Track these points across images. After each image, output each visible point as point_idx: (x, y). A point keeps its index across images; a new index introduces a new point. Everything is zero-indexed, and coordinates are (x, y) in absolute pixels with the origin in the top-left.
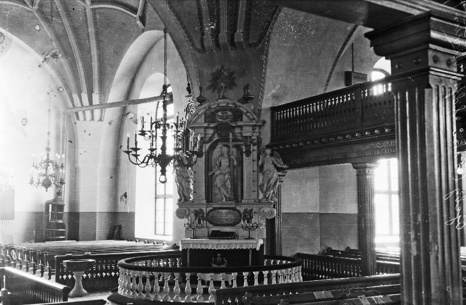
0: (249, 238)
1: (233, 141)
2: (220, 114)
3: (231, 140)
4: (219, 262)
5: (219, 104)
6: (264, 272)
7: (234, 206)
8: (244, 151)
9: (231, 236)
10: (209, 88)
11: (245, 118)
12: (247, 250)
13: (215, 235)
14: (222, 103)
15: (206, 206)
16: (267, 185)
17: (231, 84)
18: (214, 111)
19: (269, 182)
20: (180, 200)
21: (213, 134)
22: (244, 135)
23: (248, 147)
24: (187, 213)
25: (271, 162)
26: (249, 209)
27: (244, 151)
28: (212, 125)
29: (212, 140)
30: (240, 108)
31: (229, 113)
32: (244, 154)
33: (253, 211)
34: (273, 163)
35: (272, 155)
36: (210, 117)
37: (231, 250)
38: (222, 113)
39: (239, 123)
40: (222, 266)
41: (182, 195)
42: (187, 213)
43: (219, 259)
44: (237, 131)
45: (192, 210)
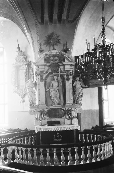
0: (71, 124)
1: (60, 73)
2: (52, 58)
3: (59, 73)
4: (58, 137)
5: (51, 53)
6: (34, 149)
7: (61, 107)
8: (66, 78)
9: (58, 123)
10: (44, 44)
11: (66, 60)
12: (73, 130)
13: (50, 123)
14: (54, 52)
16: (78, 96)
17: (58, 42)
18: (48, 56)
19: (79, 94)
20: (31, 105)
21: (49, 69)
22: (66, 69)
23: (68, 76)
25: (79, 84)
26: (70, 108)
27: (66, 78)
30: (64, 55)
31: (57, 58)
32: (66, 80)
33: (72, 110)
34: (80, 85)
35: (79, 80)
36: (47, 60)
37: (64, 131)
38: (53, 58)
40: (60, 140)
41: (31, 102)
44: (62, 67)
45: (38, 110)
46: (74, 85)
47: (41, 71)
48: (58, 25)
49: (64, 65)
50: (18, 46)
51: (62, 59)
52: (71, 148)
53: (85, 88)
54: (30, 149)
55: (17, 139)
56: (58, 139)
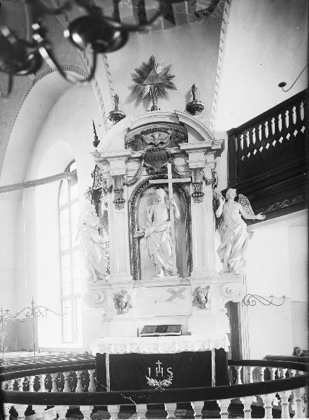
1: (173, 178)
4: (160, 374)
11: (191, 137)
14: (157, 117)
15: (132, 285)
19: (235, 242)
20: (92, 277)
22: (192, 166)
24: (101, 300)
28: (138, 154)
29: (137, 180)
32: (192, 199)
35: (236, 199)
39: (183, 146)
42: (101, 300)
43: (159, 370)
46: (218, 216)
47: (116, 178)
48: (167, 34)
49: (184, 154)
50: (96, 137)
51: (180, 133)
52: (148, 407)
53: (257, 221)
54: (67, 407)
55: (13, 381)
56: (160, 378)
